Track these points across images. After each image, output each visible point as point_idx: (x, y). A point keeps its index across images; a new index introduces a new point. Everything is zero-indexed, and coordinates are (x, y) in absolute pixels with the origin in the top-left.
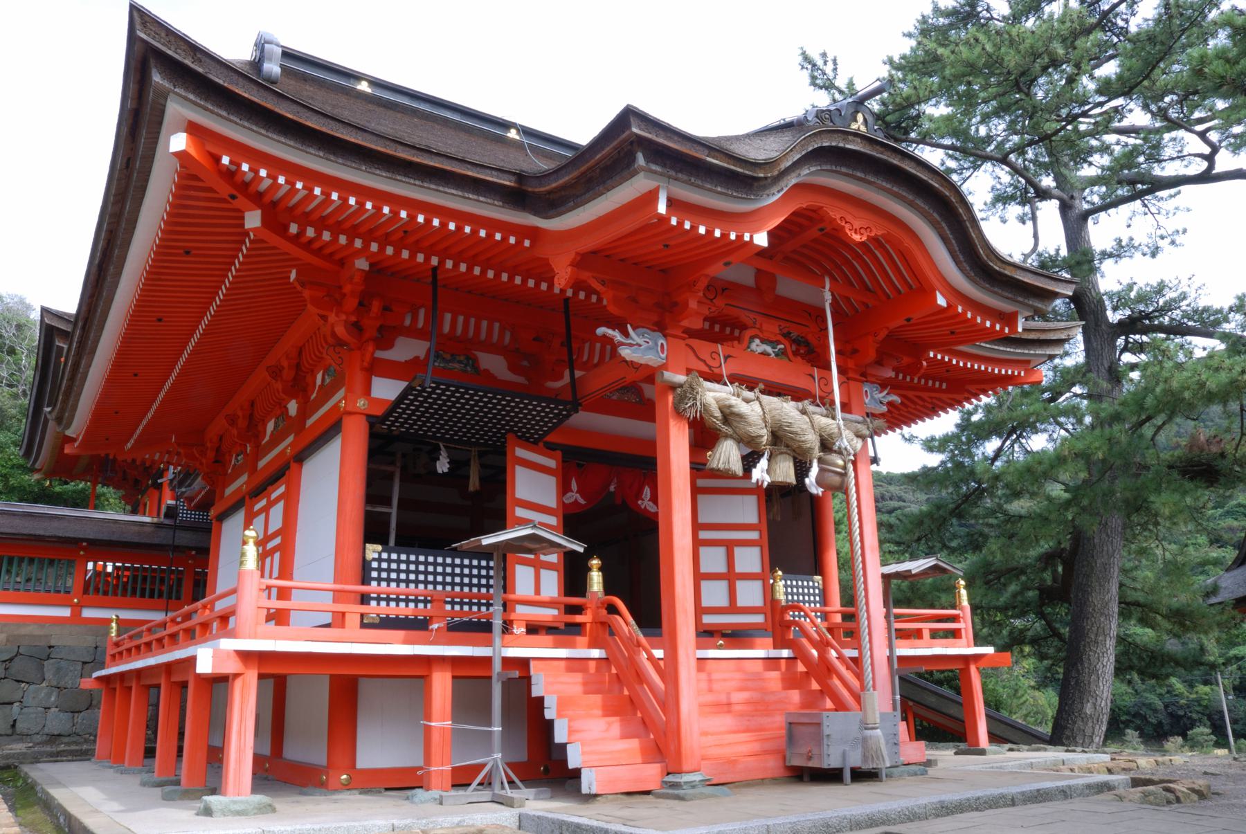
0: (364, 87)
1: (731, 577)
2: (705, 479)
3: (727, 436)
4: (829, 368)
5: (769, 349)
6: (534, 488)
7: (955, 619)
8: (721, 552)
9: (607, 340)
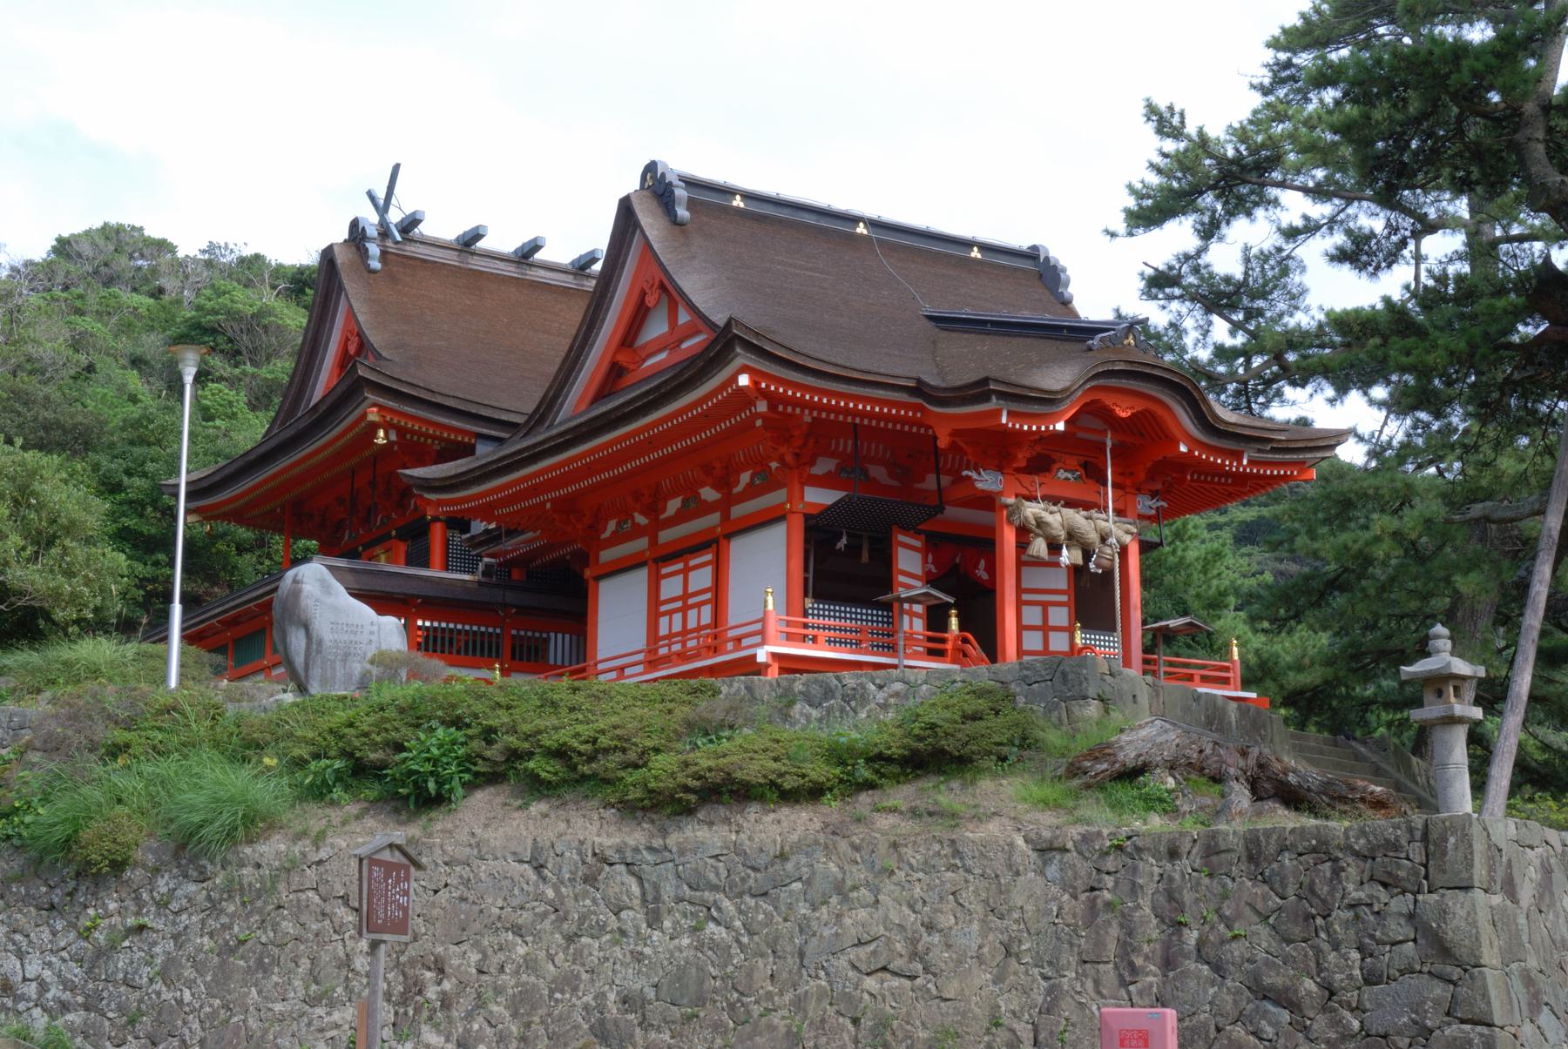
0: (738, 202)
1: (1045, 629)
2: (1024, 561)
3: (1038, 535)
4: (1105, 485)
6: (909, 561)
7: (1227, 669)
8: (1039, 609)
9: (968, 478)
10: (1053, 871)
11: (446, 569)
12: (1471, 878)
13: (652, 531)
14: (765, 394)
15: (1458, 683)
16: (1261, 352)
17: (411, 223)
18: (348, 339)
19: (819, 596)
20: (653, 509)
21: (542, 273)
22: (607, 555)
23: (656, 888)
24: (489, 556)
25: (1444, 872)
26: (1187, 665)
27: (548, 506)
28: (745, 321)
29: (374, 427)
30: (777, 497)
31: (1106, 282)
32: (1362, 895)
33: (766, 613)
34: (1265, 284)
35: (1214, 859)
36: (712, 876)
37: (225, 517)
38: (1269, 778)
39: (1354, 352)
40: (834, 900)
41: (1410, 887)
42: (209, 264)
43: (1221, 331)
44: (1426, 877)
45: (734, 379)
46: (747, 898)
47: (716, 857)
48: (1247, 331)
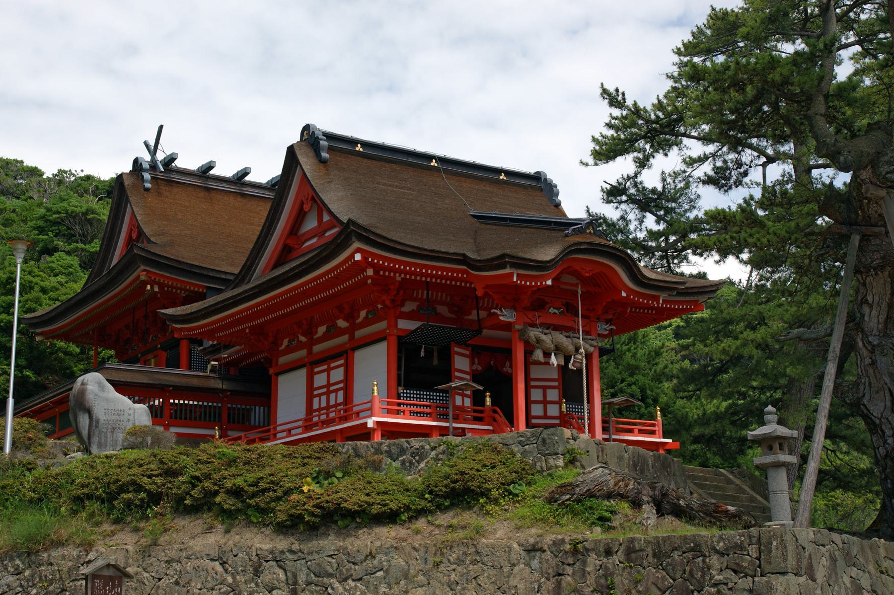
1: (545, 402)
5: (556, 311)
6: (461, 363)
8: (540, 391)
9: (495, 314)
10: (535, 563)
11: (190, 369)
12: (786, 567)
13: (309, 346)
14: (371, 265)
15: (781, 441)
16: (674, 234)
17: (172, 159)
18: (132, 230)
19: (406, 387)
20: (310, 332)
21: (249, 189)
22: (282, 360)
23: (295, 576)
24: (214, 360)
25: (770, 563)
26: (628, 423)
27: (247, 331)
28: (360, 222)
29: (145, 283)
30: (383, 325)
31: (582, 193)
32: (721, 577)
33: (373, 397)
34: (676, 193)
35: (633, 555)
36: (328, 568)
37: (59, 337)
38: (668, 502)
39: (725, 232)
40: (403, 582)
41: (750, 573)
42: (60, 182)
43: (650, 222)
44: (759, 566)
45: (352, 256)
46: (350, 581)
47: (330, 556)
48: (665, 221)
